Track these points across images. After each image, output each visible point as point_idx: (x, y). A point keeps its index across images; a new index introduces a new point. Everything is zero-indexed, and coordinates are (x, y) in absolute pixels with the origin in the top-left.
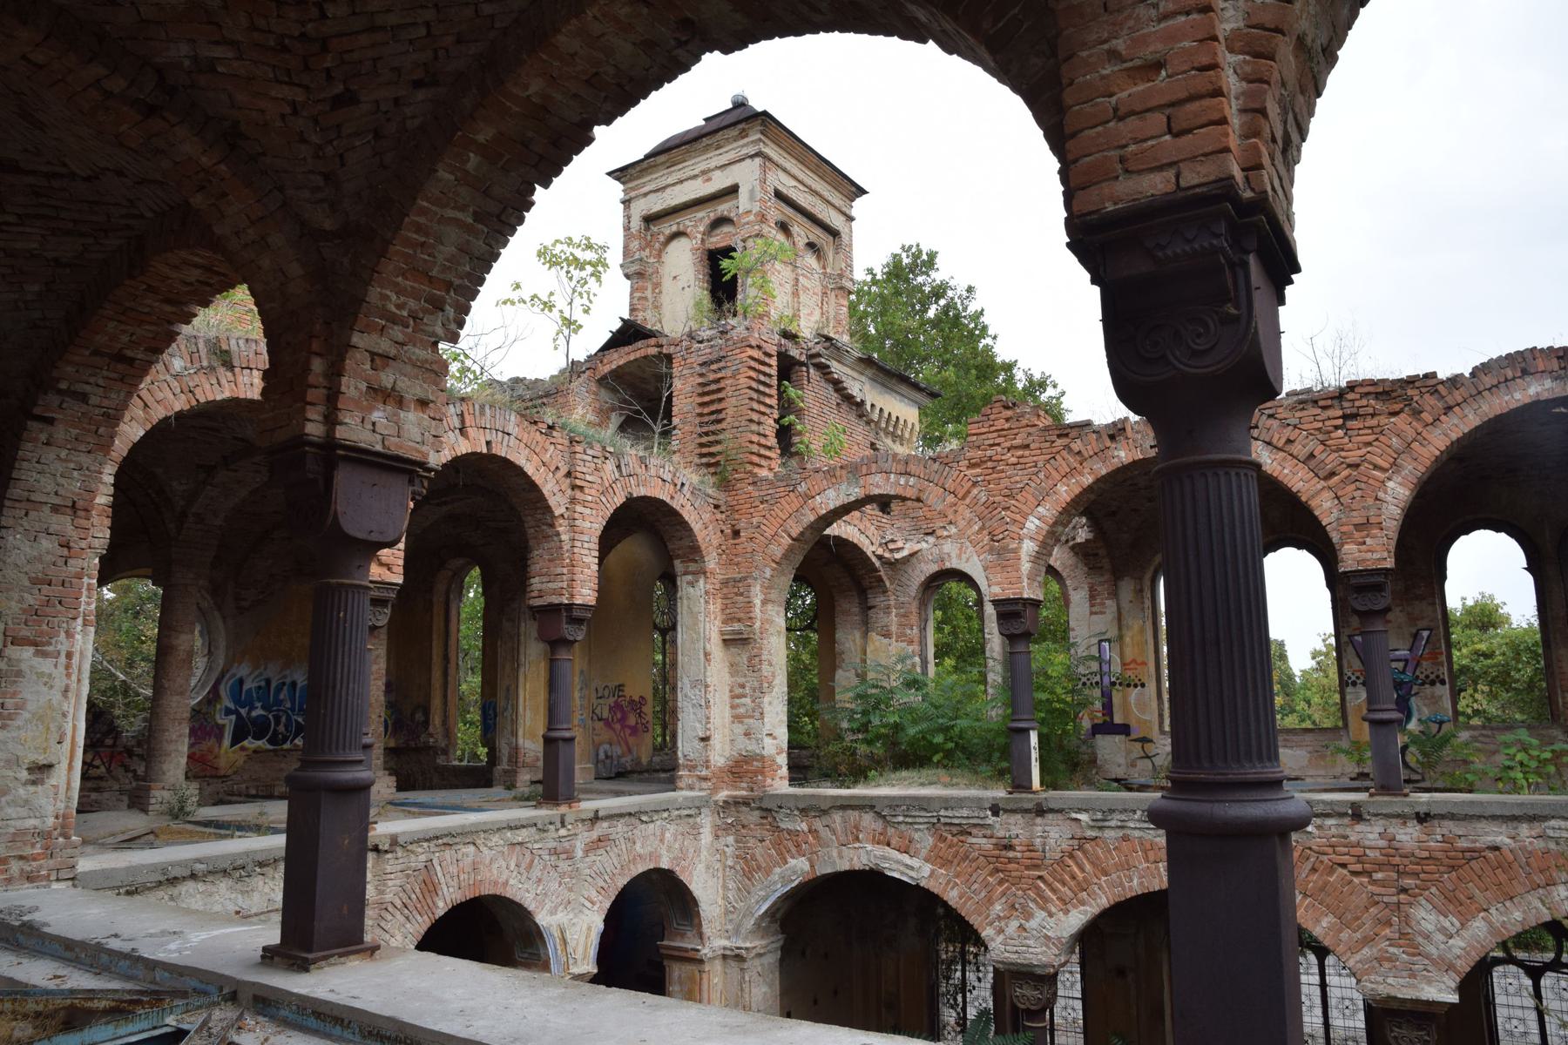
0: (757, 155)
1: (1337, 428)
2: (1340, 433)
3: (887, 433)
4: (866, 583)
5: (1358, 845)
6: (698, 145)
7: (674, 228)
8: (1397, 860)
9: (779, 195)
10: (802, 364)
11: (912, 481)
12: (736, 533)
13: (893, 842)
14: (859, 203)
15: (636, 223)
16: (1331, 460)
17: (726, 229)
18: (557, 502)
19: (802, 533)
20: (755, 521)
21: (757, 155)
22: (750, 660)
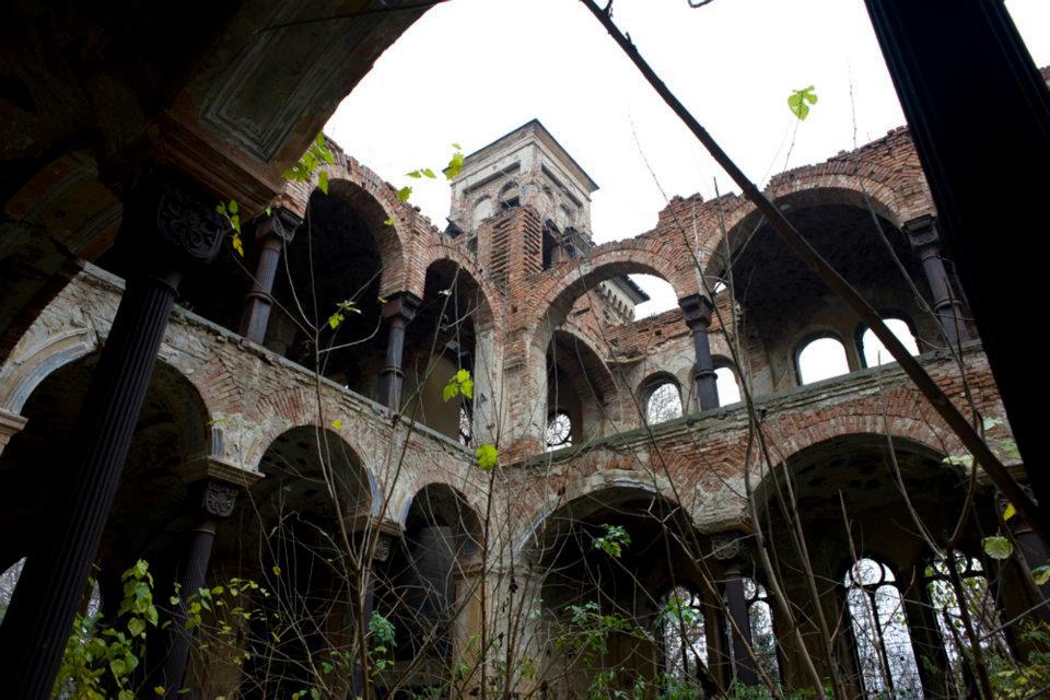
0: (531, 143)
1: (885, 155)
2: (888, 157)
3: (615, 309)
4: (602, 388)
5: (946, 378)
6: (496, 146)
7: (482, 194)
8: (977, 380)
9: (544, 170)
10: (558, 245)
11: (625, 252)
12: (515, 310)
13: (621, 464)
14: (593, 195)
15: (459, 193)
16: (885, 172)
17: (513, 190)
18: (403, 236)
19: (556, 299)
20: (527, 299)
21: (531, 143)
22: (522, 378)
